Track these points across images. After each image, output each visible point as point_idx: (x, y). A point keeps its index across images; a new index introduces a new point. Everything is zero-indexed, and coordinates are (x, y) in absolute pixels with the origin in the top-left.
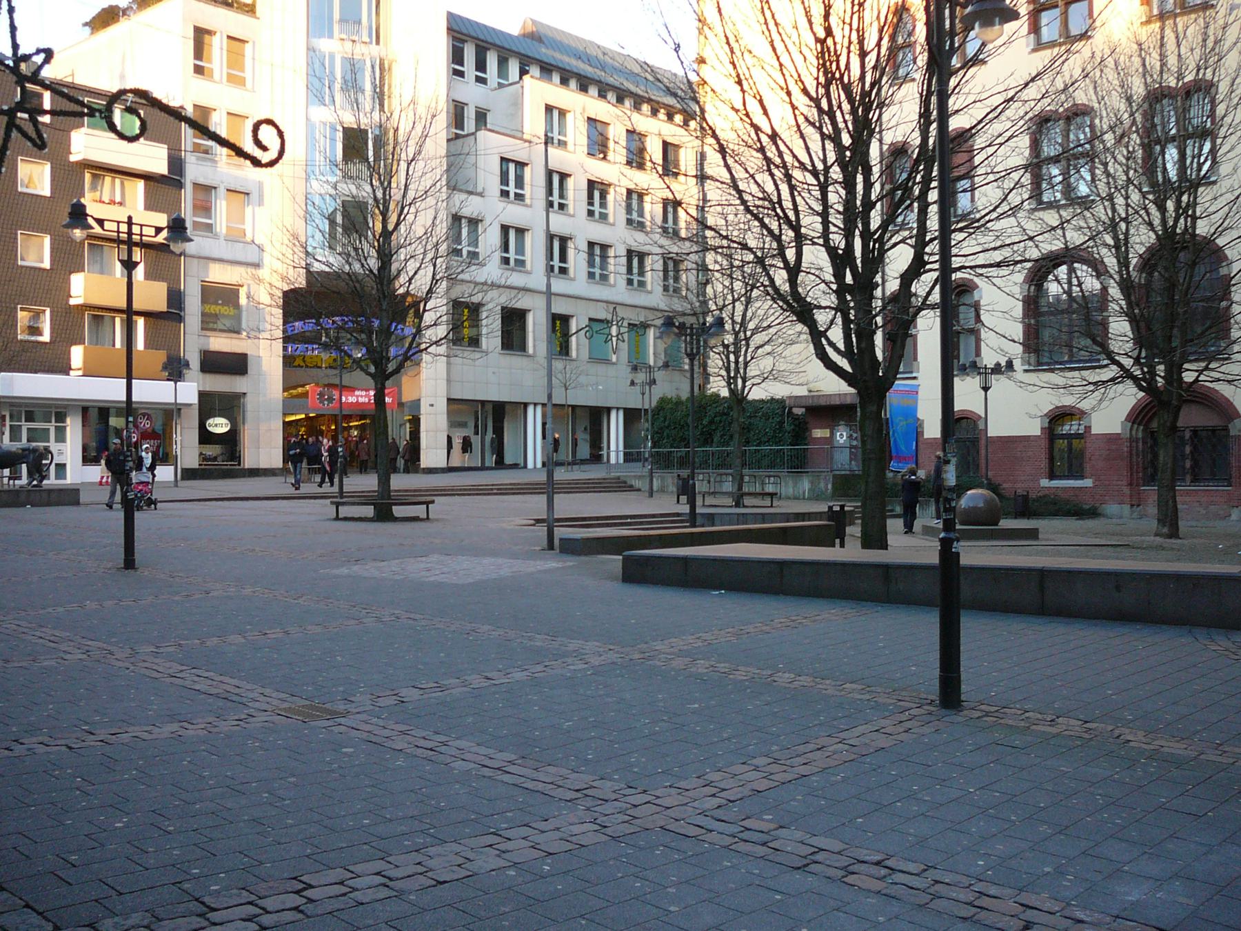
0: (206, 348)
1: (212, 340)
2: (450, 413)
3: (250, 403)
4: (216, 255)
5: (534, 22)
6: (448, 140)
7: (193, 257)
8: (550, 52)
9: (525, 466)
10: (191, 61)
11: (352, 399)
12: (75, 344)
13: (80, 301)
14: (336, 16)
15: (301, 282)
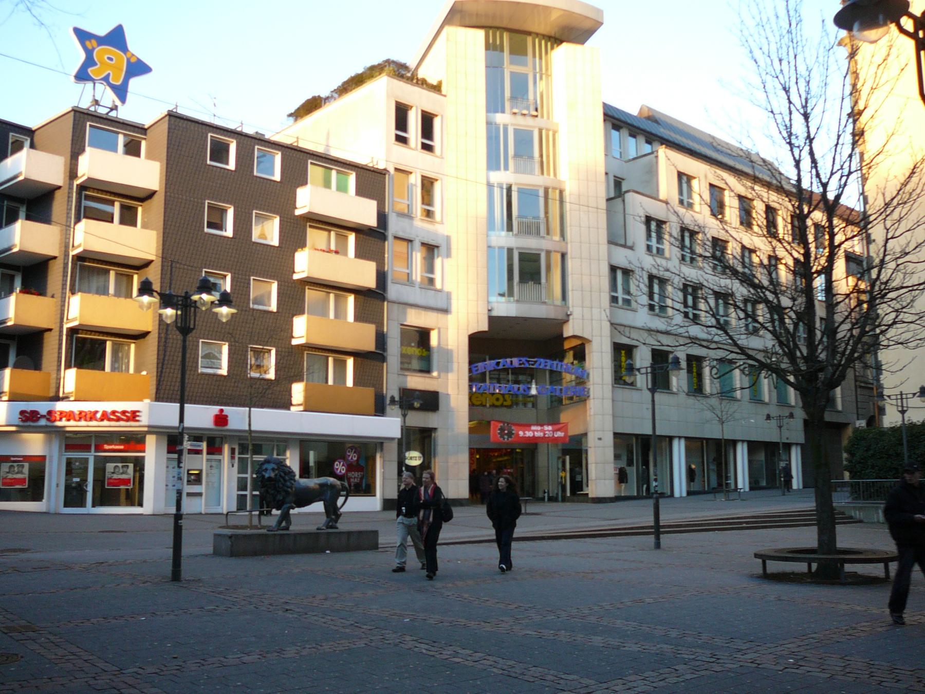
0: (403, 386)
1: (409, 378)
2: (616, 446)
3: (441, 438)
4: (411, 300)
5: (649, 109)
6: (608, 200)
7: (394, 302)
8: (662, 130)
9: (672, 495)
10: (393, 131)
11: (529, 434)
12: (296, 381)
13: (302, 341)
14: (507, 93)
15: (484, 327)
